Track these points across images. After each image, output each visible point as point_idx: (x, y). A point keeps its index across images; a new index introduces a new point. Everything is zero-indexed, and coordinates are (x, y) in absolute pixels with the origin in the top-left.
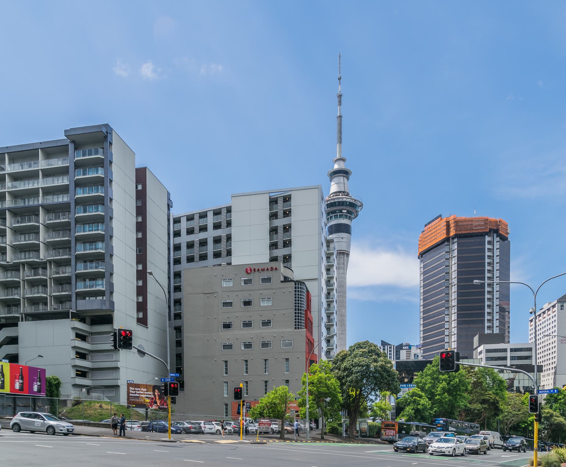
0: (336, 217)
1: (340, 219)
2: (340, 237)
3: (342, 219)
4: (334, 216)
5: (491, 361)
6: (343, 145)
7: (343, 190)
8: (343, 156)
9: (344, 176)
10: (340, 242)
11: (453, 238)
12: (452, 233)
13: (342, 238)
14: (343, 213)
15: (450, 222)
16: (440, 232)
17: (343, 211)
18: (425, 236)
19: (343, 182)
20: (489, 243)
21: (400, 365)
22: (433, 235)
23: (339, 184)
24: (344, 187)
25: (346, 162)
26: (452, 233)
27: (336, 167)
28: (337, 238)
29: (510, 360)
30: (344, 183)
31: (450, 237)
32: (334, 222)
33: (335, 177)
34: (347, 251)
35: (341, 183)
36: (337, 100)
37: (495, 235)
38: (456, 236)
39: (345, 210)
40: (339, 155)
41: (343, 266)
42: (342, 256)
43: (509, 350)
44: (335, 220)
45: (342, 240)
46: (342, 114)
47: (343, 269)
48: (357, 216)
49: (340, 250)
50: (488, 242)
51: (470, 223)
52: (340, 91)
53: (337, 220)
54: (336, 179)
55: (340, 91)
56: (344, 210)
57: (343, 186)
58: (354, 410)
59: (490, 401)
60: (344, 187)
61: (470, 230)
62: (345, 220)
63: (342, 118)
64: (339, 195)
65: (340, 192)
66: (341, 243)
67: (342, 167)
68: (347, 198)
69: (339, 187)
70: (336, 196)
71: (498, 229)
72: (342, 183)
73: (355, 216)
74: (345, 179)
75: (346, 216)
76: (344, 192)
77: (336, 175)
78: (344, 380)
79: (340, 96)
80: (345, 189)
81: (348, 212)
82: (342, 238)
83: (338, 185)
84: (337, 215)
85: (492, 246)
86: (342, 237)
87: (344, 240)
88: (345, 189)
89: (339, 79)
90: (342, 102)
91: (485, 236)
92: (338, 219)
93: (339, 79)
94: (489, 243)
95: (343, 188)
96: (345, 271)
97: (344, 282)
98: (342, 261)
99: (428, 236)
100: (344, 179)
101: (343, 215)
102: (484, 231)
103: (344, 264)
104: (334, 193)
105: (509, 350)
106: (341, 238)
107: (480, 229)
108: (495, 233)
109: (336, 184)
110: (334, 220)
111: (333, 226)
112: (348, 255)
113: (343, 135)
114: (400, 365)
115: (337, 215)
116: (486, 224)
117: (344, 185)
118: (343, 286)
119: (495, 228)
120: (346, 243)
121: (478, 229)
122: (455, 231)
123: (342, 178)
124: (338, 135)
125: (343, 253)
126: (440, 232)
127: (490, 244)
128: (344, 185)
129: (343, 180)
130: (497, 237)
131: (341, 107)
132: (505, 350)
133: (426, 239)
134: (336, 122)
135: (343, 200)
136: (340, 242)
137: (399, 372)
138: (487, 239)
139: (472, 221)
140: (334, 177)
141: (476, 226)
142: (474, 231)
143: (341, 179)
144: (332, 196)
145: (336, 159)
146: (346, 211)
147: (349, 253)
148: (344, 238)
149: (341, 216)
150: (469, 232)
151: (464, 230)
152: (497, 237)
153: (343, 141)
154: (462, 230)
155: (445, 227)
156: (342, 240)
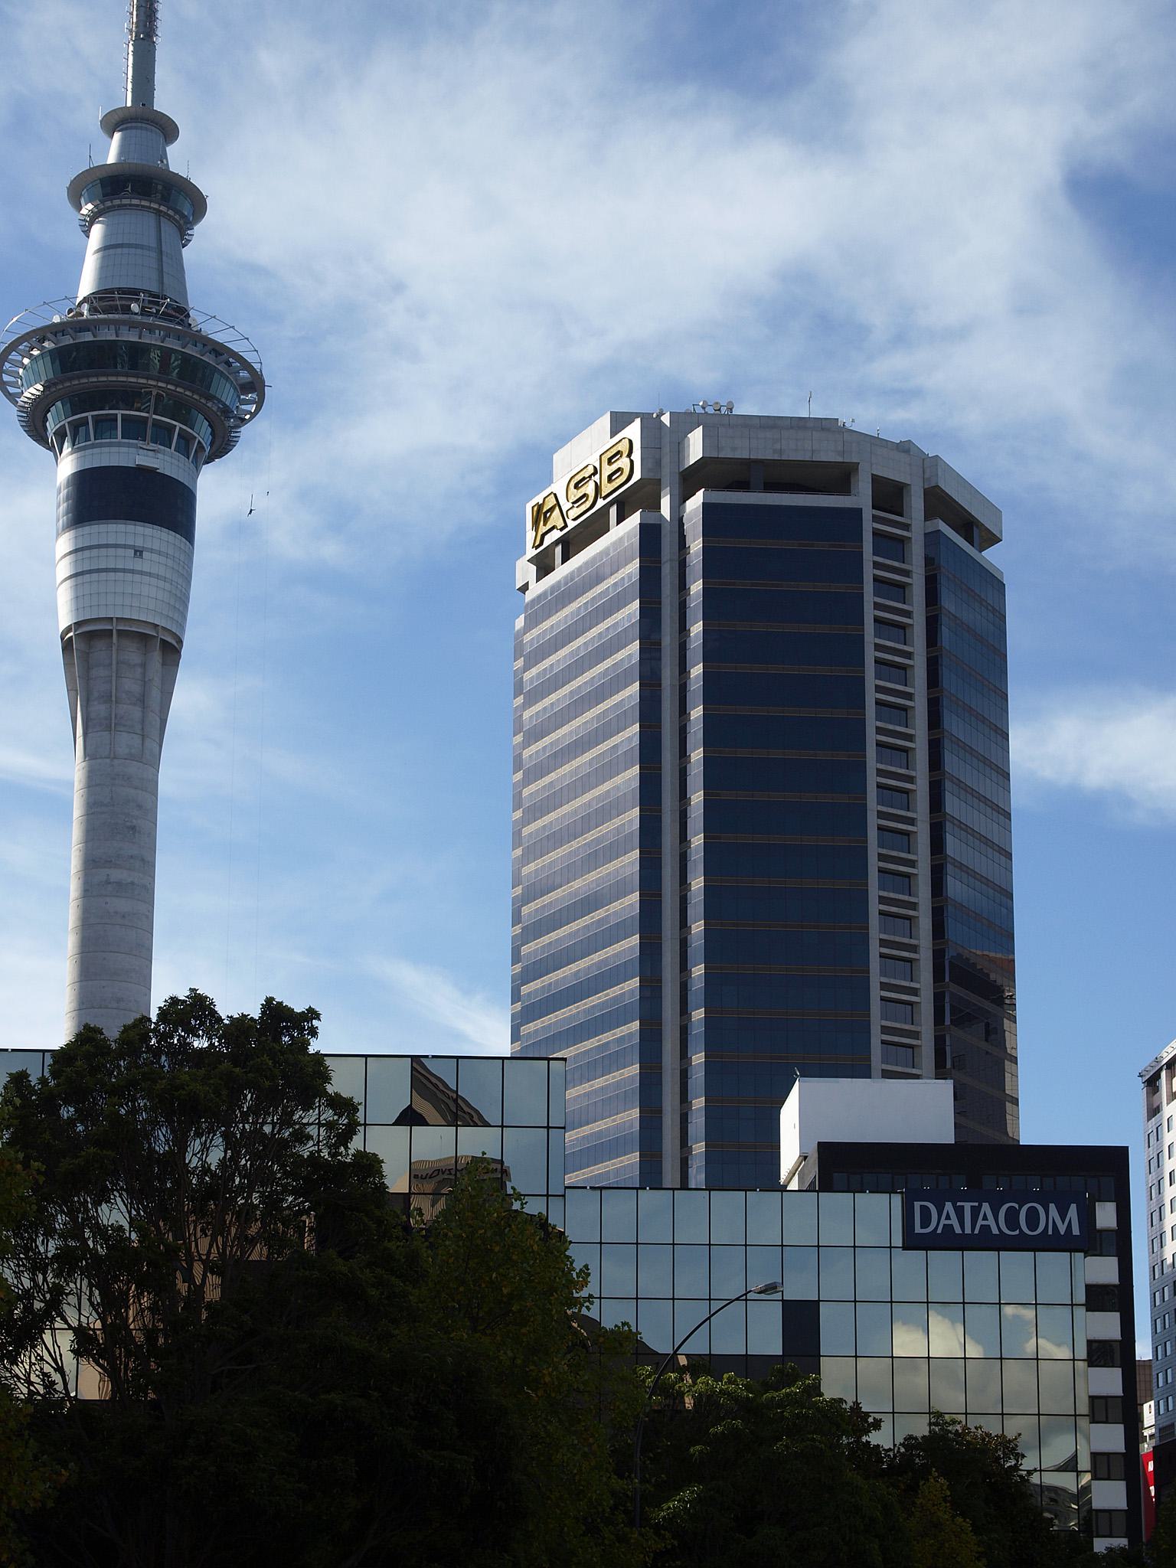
2: (125, 547)
4: (97, 421)
19: (154, 244)
41: (136, 712)
44: (101, 445)
45: (138, 565)
47: (139, 732)
53: (110, 445)
72: (149, 248)
86: (139, 543)
88: (162, 283)
92: (119, 445)
97: (140, 807)
112: (171, 650)
118: (133, 828)
147: (180, 642)
148: (152, 551)
156: (138, 565)
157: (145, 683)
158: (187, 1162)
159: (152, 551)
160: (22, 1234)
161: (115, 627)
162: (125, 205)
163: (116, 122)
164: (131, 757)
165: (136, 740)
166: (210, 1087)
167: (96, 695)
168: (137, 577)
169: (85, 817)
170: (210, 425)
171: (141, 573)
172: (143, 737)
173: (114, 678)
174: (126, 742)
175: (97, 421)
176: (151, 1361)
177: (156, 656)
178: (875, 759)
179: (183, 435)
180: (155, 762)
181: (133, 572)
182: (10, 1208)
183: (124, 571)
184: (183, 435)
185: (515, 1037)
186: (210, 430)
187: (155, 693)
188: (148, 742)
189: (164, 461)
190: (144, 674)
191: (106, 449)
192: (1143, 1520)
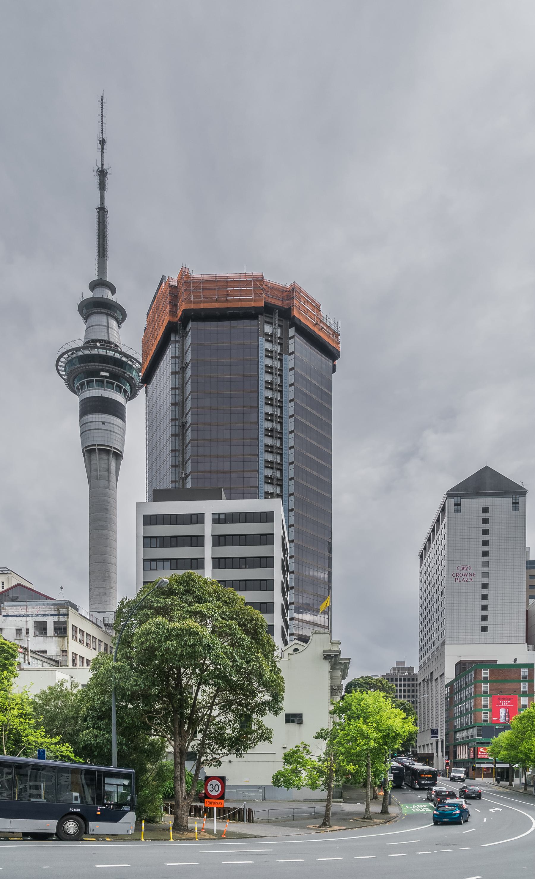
2: (99, 421)
3: (101, 390)
4: (88, 382)
5: (160, 547)
7: (106, 338)
14: (102, 376)
17: (102, 373)
19: (106, 324)
21: (375, 761)
29: (213, 545)
35: (102, 325)
39: (106, 372)
41: (106, 474)
42: (104, 457)
43: (208, 520)
44: (89, 390)
45: (103, 427)
47: (107, 479)
49: (98, 445)
53: (92, 390)
56: (103, 371)
57: (106, 331)
58: (312, 821)
67: (104, 297)
71: (290, 308)
72: (104, 326)
86: (103, 420)
92: (95, 389)
95: (106, 334)
97: (109, 503)
100: (322, 801)
102: (253, 304)
103: (108, 470)
105: (208, 520)
106: (101, 423)
107: (243, 300)
110: (87, 391)
114: (375, 761)
115: (92, 381)
119: (283, 305)
125: (108, 452)
132: (198, 519)
137: (192, 686)
142: (227, 305)
146: (107, 374)
148: (108, 423)
150: (217, 305)
151: (205, 302)
156: (103, 427)
159: (108, 423)
160: (169, 681)
161: (96, 447)
162: (96, 312)
163: (93, 286)
165: (107, 482)
167: (93, 469)
170: (130, 385)
171: (105, 430)
173: (98, 463)
174: (103, 483)
178: (484, 593)
179: (117, 385)
182: (222, 711)
183: (99, 429)
184: (117, 385)
185: (84, 345)
186: (129, 387)
190: (108, 462)
191: (91, 391)
192: (396, 832)
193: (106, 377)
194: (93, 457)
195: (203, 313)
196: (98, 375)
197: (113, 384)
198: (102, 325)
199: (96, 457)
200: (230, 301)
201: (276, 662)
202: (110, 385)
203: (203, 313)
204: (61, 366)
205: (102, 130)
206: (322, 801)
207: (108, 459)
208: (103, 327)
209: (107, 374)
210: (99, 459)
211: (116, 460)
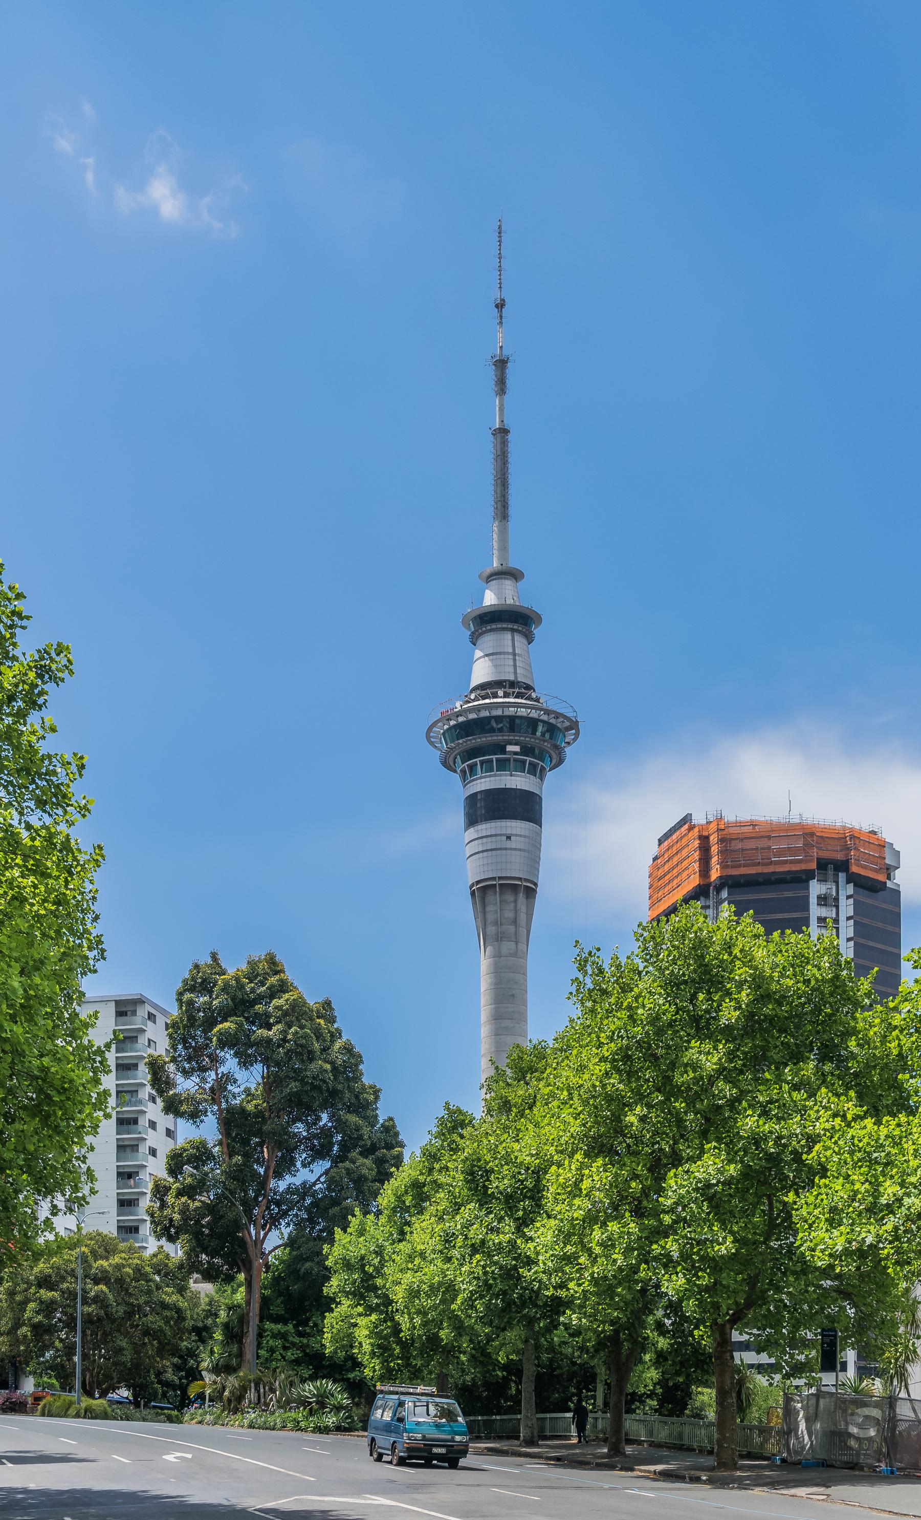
0: (488, 766)
1: (501, 775)
2: (501, 835)
3: (506, 775)
4: (482, 763)
6: (511, 524)
7: (512, 678)
8: (513, 564)
9: (513, 631)
10: (501, 849)
11: (718, 889)
12: (715, 875)
13: (509, 838)
15: (711, 838)
16: (687, 868)
17: (510, 748)
18: (660, 871)
19: (510, 650)
20: (823, 900)
22: (683, 864)
23: (502, 656)
24: (515, 666)
25: (519, 584)
26: (715, 875)
27: (490, 599)
28: (491, 836)
30: (514, 654)
31: (709, 885)
32: (484, 783)
33: (491, 630)
34: (527, 880)
35: (504, 653)
36: (491, 373)
37: (842, 877)
38: (726, 882)
39: (516, 744)
40: (499, 558)
41: (512, 929)
42: (510, 897)
45: (509, 844)
46: (508, 424)
47: (513, 939)
48: (560, 761)
49: (500, 878)
50: (819, 897)
51: (763, 843)
52: (501, 347)
53: (490, 776)
54: (489, 641)
55: (501, 347)
56: (511, 744)
57: (511, 662)
59: (176, 1360)
60: (515, 666)
61: (764, 865)
62: (515, 776)
63: (510, 437)
64: (495, 696)
65: (499, 684)
66: (504, 852)
67: (508, 602)
68: (518, 705)
69: (495, 666)
70: (484, 698)
72: (508, 653)
73: (554, 762)
74: (520, 640)
75: (519, 764)
76: (512, 684)
77: (489, 628)
78: (850, 1309)
79: (501, 364)
80: (515, 673)
81: (527, 750)
82: (509, 838)
83: (492, 660)
84: (491, 761)
85: (834, 910)
86: (509, 832)
87: (515, 843)
88: (515, 673)
89: (500, 306)
90: (509, 383)
91: (807, 881)
92: (495, 776)
93: (497, 306)
94: (823, 900)
95: (511, 670)
96: (522, 946)
97: (516, 983)
98: (509, 914)
99: (665, 875)
100: (513, 640)
101: (508, 760)
102: (804, 867)
103: (515, 922)
104: (482, 687)
107: (791, 862)
108: (842, 871)
109: (487, 655)
110: (481, 778)
111: (479, 797)
112: (530, 892)
113: (512, 490)
115: (491, 761)
116: (807, 845)
117: (515, 660)
118: (513, 996)
119: (840, 856)
120: (526, 854)
121: (786, 862)
122: (722, 868)
123: (508, 636)
124: (496, 492)
125: (515, 888)
126: (687, 868)
127: (825, 905)
128: (515, 660)
129: (510, 643)
130: (848, 882)
131: (505, 397)
133: (661, 882)
134: (488, 446)
135: (506, 713)
136: (501, 849)
138: (816, 888)
139: (769, 837)
140: (484, 633)
141: (781, 852)
143: (505, 640)
144: (473, 697)
145: (489, 571)
146: (517, 748)
147: (536, 884)
148: (516, 835)
149: (503, 765)
150: (759, 869)
152: (848, 882)
153: (512, 511)
154: (739, 866)
155: (698, 853)
156: (509, 844)
157: (516, 911)
158: (624, 1358)
164: (510, 955)
165: (513, 945)
166: (887, 1003)
168: (509, 852)
169: (493, 1006)
171: (511, 849)
172: (517, 943)
174: (508, 946)
175: (482, 763)
176: (539, 1327)
177: (521, 896)
180: (525, 956)
181: (506, 849)
187: (523, 917)
188: (520, 944)
189: (518, 781)
190: (516, 906)
193: (515, 753)
194: (490, 898)
195: (742, 881)
196: (503, 751)
197: (524, 762)
198: (504, 653)
199: (493, 899)
200: (777, 863)
201: (397, 1317)
202: (521, 766)
203: (742, 881)
204: (433, 737)
205: (500, 283)
206: (513, 640)
207: (515, 901)
208: (506, 656)
209: (517, 748)
210: (501, 901)
211: (527, 897)
